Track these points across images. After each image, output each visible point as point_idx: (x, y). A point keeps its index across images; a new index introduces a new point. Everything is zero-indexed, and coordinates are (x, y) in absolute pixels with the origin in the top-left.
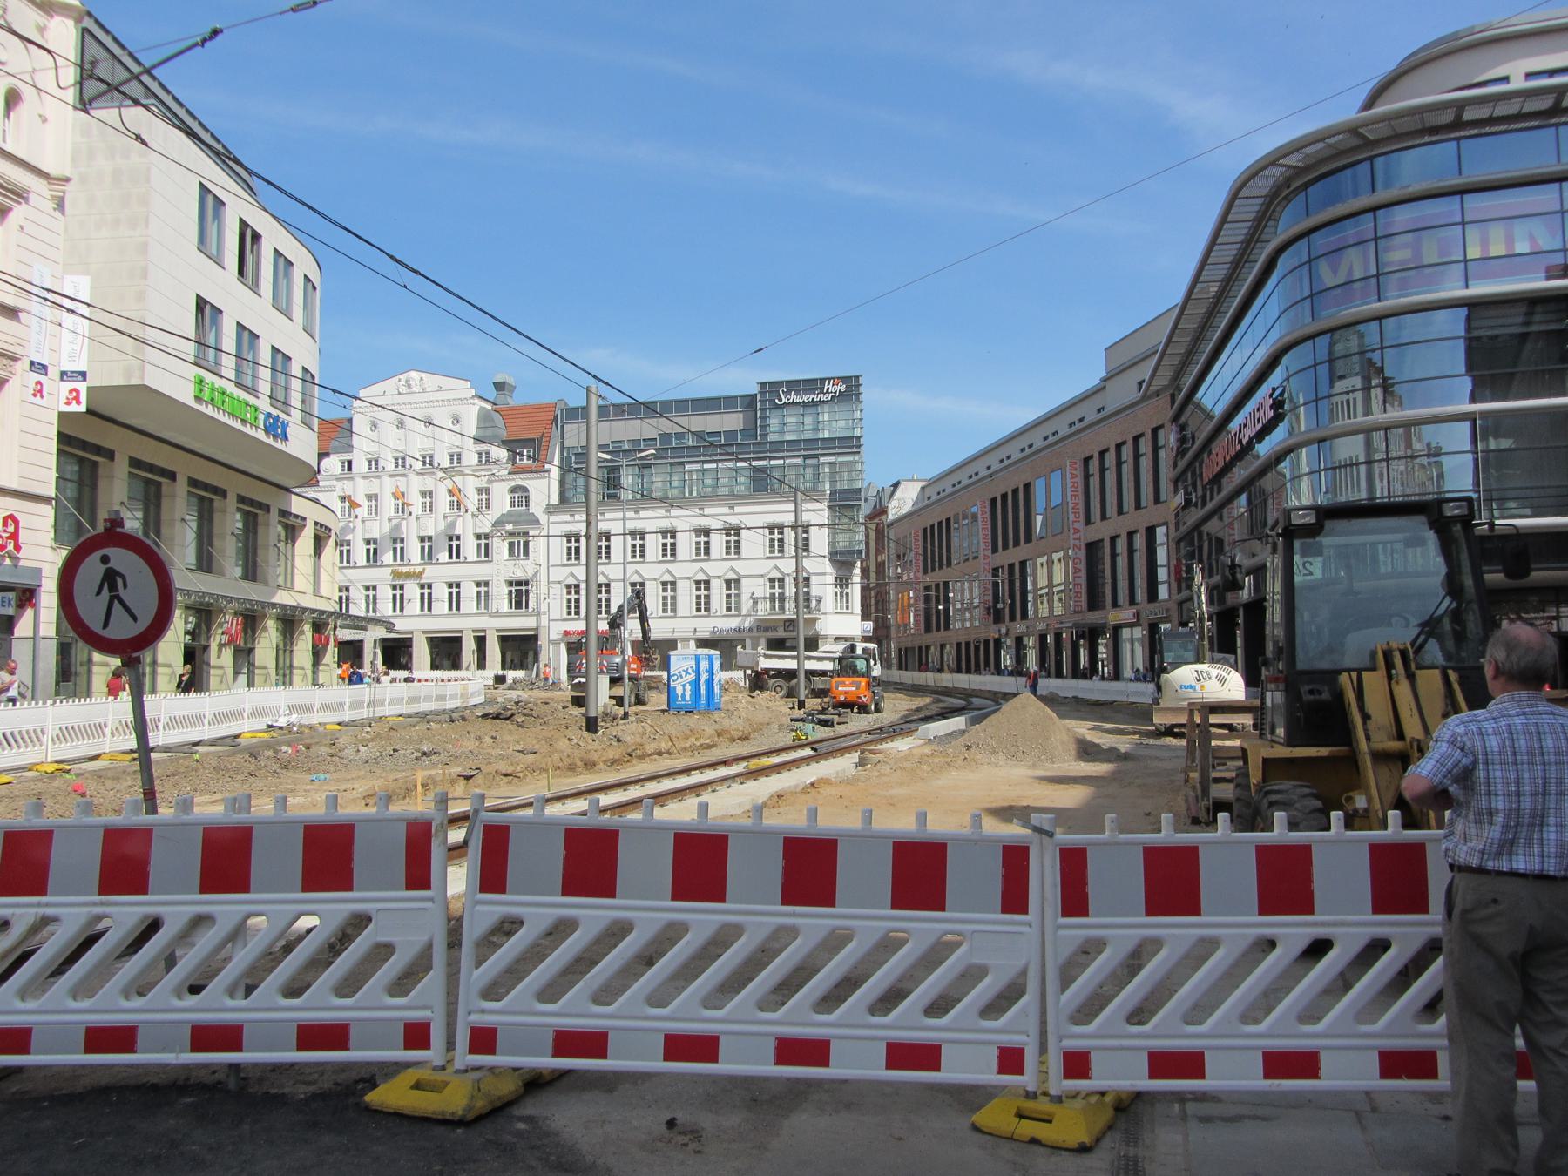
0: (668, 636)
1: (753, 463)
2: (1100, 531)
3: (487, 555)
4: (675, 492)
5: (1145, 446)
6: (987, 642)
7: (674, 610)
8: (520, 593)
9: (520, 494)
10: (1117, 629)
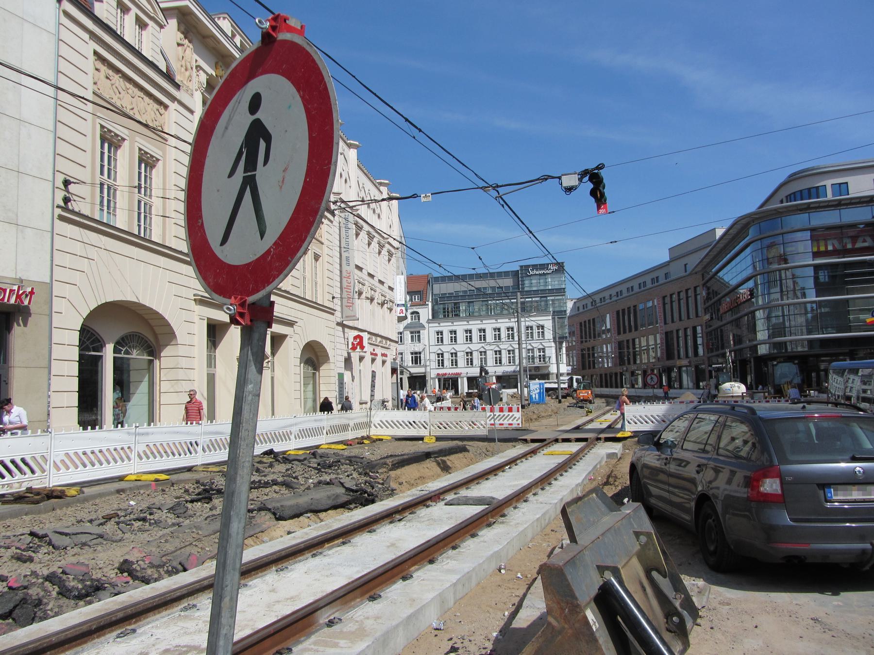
1: (512, 301)
2: (672, 327)
4: (484, 313)
5: (691, 293)
6: (616, 374)
8: (417, 358)
9: (415, 315)
10: (680, 368)
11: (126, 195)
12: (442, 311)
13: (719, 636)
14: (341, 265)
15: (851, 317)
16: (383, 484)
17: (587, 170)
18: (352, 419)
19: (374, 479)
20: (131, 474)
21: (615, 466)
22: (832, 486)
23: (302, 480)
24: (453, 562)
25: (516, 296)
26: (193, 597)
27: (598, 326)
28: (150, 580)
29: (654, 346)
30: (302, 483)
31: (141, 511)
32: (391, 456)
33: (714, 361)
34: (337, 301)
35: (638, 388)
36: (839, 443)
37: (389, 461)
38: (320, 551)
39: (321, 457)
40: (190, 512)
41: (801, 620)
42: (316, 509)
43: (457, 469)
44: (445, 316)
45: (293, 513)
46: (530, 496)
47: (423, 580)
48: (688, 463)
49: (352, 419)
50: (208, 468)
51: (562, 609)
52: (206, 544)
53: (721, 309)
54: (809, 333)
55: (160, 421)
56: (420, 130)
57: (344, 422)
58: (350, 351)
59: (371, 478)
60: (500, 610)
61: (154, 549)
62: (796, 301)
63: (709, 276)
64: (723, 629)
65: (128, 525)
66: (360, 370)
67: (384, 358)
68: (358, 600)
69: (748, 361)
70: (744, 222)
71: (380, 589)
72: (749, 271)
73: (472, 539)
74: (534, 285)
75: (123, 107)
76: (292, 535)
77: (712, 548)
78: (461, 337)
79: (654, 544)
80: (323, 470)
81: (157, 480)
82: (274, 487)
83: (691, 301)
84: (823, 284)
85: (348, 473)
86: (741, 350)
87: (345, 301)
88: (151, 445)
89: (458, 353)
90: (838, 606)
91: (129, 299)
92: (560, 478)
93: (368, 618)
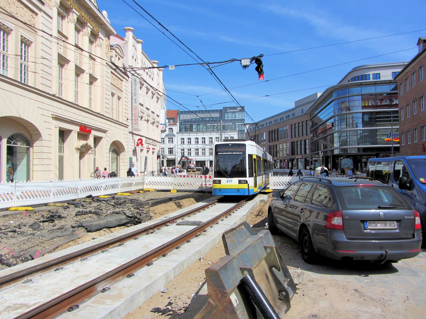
0: (203, 160)
2: (294, 140)
3: (163, 142)
4: (205, 130)
5: (304, 124)
7: (205, 155)
8: (171, 151)
9: (171, 130)
10: (298, 159)
11: (14, 60)
12: (184, 128)
13: (307, 300)
14: (132, 103)
15: (378, 137)
16: (146, 214)
17: (255, 57)
18: (134, 181)
19: (142, 211)
20: (13, 207)
21: (263, 206)
22: (368, 222)
23: (104, 211)
24: (175, 256)
25: (220, 122)
26: (31, 275)
27: (259, 138)
28: (11, 265)
29: (286, 149)
30: (104, 212)
31: (15, 226)
32: (152, 199)
33: (313, 157)
34: (130, 121)
35: (278, 168)
36: (372, 199)
37: (150, 202)
38: (106, 249)
39: (117, 199)
40: (41, 228)
41: (349, 290)
42: (109, 226)
43: (185, 206)
44: (185, 131)
45: (96, 229)
46: (220, 221)
47: (158, 266)
48: (297, 207)
49: (134, 181)
50: (56, 204)
51: (217, 295)
52: (47, 245)
53: (318, 132)
54: (358, 144)
55: (33, 180)
56: (167, 30)
57: (130, 182)
58: (136, 146)
59: (140, 210)
60: (197, 281)
61: (16, 248)
62: (353, 129)
63: (313, 116)
64: (309, 295)
65: (5, 234)
66: (141, 156)
67: (154, 150)
68: (121, 277)
69: (329, 157)
70: (331, 90)
71: (134, 271)
72: (332, 114)
73: (187, 243)
74: (229, 117)
75: (11, 12)
76: (94, 240)
77: (306, 251)
78: (193, 141)
79: (274, 253)
80: (116, 206)
81: (27, 210)
82: (90, 214)
83: (304, 127)
84: (366, 122)
85: (129, 208)
86: (326, 152)
87: (133, 121)
88: (24, 192)
89: (192, 149)
90: (367, 282)
91: (15, 115)
92: (235, 212)
93: (125, 287)
